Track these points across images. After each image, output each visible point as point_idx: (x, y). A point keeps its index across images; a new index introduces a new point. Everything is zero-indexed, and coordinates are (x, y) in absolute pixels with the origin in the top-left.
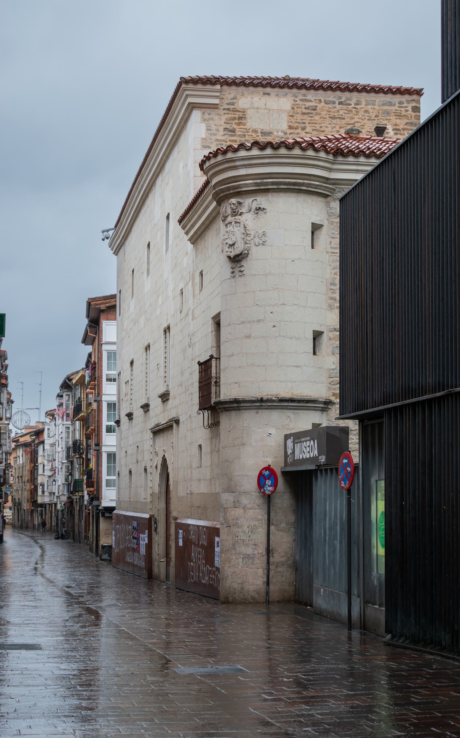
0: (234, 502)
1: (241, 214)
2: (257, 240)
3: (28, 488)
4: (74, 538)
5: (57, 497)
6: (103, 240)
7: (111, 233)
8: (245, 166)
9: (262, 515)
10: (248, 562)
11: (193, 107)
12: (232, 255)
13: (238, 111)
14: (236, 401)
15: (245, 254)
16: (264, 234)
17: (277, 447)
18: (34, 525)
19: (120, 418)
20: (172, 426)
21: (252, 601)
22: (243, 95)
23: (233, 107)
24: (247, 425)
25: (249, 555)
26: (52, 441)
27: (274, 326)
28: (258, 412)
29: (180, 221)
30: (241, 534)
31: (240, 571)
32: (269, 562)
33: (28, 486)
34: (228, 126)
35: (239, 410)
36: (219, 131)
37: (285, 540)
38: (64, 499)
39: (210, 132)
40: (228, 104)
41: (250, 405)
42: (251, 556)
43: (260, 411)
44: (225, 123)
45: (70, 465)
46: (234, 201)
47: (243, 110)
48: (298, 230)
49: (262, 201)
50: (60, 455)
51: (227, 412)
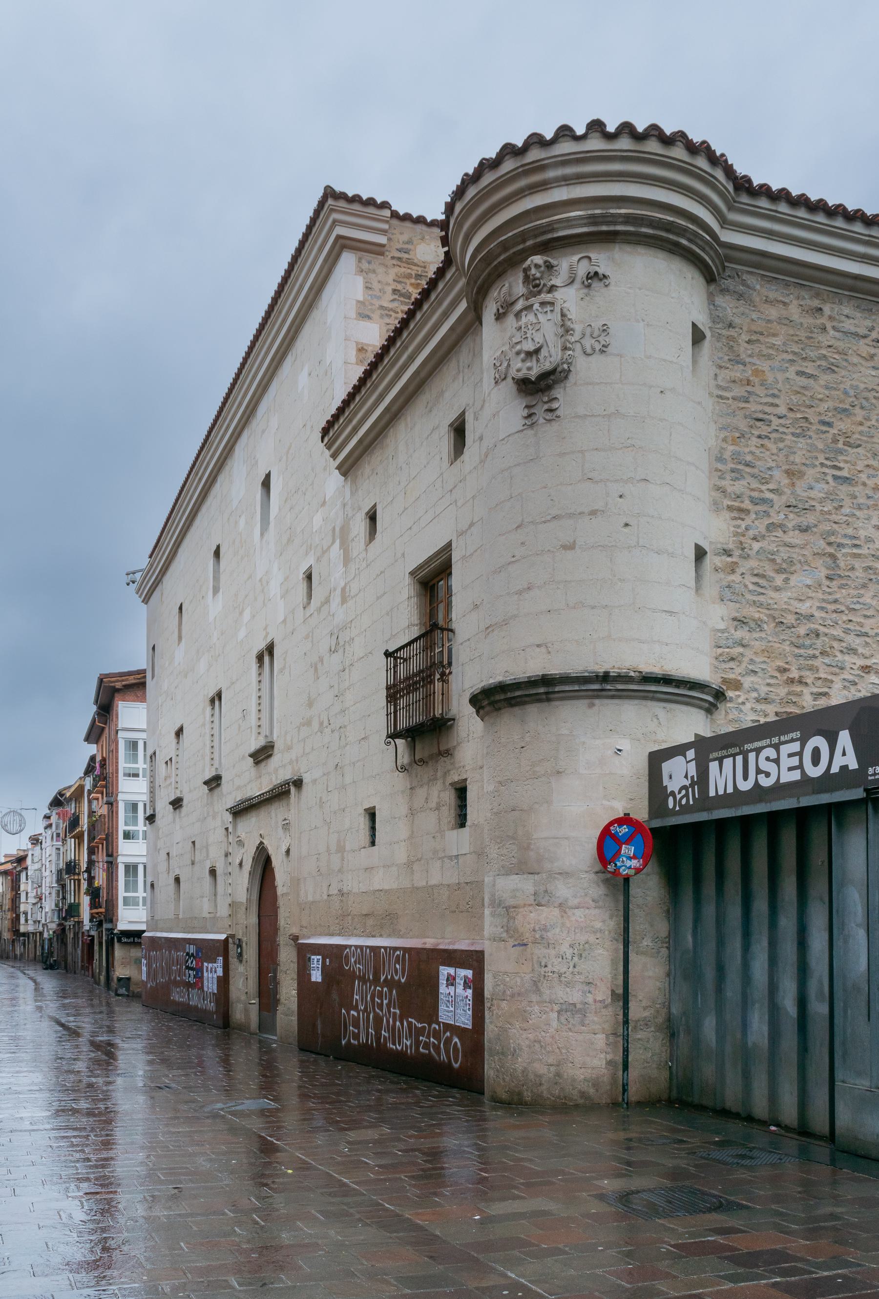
0: (535, 894)
1: (552, 289)
2: (588, 343)
3: (9, 917)
4: (66, 968)
5: (43, 925)
6: (128, 584)
7: (138, 576)
8: (567, 181)
9: (604, 921)
10: (570, 1019)
11: (343, 244)
12: (533, 374)
13: (416, 265)
14: (546, 681)
15: (564, 370)
16: (605, 329)
17: (634, 778)
18: (16, 956)
19: (154, 811)
20: (288, 792)
21: (581, 1101)
22: (423, 239)
23: (406, 256)
24: (566, 732)
25: (574, 1005)
26: (37, 866)
27: (627, 525)
28: (593, 705)
29: (325, 431)
30: (554, 960)
31: (553, 1037)
32: (628, 1019)
33: (9, 915)
34: (399, 287)
35: (549, 700)
36: (385, 293)
37: (650, 974)
38: (53, 926)
39: (370, 292)
40: (399, 250)
41: (576, 688)
42: (578, 1006)
43: (597, 701)
44: (394, 280)
45: (60, 889)
46: (538, 259)
47: (422, 265)
48: (670, 331)
49: (602, 259)
50: (48, 880)
51: (516, 710)
